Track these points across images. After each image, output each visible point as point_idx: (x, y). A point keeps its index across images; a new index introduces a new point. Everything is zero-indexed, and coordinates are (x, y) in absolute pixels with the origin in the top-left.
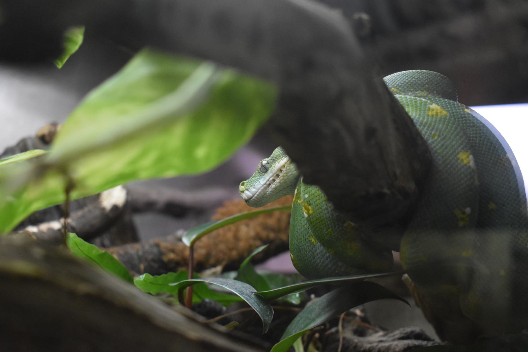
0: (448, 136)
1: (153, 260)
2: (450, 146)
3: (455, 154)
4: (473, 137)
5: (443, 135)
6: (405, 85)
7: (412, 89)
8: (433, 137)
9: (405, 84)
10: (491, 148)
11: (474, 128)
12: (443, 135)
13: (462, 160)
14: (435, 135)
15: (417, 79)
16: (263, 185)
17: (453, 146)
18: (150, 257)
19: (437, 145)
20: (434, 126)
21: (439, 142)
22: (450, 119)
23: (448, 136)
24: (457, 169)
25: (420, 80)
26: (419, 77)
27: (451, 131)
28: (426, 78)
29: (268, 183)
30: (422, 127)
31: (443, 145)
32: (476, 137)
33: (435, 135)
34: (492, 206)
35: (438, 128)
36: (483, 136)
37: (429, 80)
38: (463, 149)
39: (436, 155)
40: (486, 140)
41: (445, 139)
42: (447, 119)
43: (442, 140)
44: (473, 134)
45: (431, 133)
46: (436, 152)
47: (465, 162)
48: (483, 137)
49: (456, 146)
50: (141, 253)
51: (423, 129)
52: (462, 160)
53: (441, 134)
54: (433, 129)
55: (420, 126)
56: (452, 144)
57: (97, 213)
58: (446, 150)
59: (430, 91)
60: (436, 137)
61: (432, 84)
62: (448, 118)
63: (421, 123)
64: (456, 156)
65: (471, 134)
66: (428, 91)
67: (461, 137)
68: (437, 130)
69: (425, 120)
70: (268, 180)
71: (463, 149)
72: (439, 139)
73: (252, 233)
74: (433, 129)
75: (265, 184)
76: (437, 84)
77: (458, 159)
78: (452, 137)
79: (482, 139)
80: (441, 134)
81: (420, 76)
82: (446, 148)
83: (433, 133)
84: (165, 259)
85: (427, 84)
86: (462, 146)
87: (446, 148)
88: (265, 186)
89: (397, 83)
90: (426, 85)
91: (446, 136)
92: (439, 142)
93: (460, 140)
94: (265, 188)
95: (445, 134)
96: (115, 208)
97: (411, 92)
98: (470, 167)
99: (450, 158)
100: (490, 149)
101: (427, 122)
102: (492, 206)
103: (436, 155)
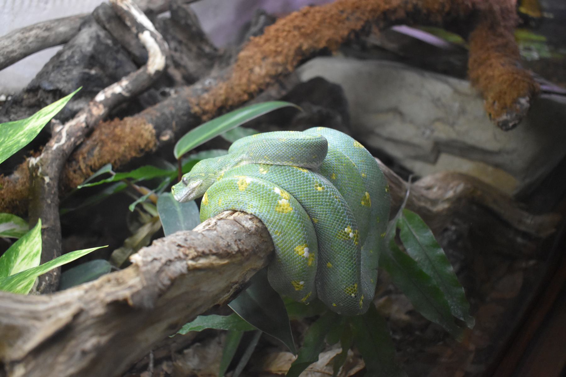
0: (289, 232)
1: (184, 115)
2: (289, 241)
3: (292, 247)
4: (320, 214)
5: (284, 231)
6: (275, 156)
7: (279, 160)
8: (276, 234)
9: (274, 156)
10: (334, 224)
11: (322, 206)
12: (284, 231)
13: (298, 252)
14: (277, 232)
15: (284, 152)
16: (185, 195)
17: (292, 241)
18: (181, 113)
19: (278, 240)
20: (278, 224)
21: (280, 238)
22: (292, 217)
23: (289, 232)
24: (293, 258)
25: (286, 154)
26: (286, 151)
27: (292, 228)
28: (292, 152)
29: (188, 194)
30: (268, 224)
31: (283, 240)
32: (322, 214)
33: (277, 232)
34: (329, 265)
35: (281, 225)
36: (328, 214)
37: (294, 154)
38: (299, 243)
39: (277, 247)
40: (330, 217)
41: (286, 235)
42: (290, 216)
43: (282, 236)
44: (320, 211)
45: (274, 230)
46: (277, 245)
47: (300, 253)
48: (328, 214)
49: (294, 241)
50: (173, 111)
51: (269, 225)
52: (298, 252)
53: (283, 231)
54: (277, 226)
55: (267, 223)
56: (291, 239)
57: (145, 77)
58: (286, 244)
59: (294, 162)
60: (278, 234)
61: (297, 156)
62: (291, 215)
63: (268, 221)
64: (293, 248)
65: (318, 212)
66: (293, 162)
67: (300, 233)
68: (280, 228)
69: (271, 218)
70: (188, 192)
71: (299, 243)
72: (281, 235)
73: (263, 72)
74: (277, 226)
75: (186, 194)
76: (301, 156)
77: (294, 251)
78: (291, 233)
79: (327, 216)
80: (283, 231)
81: (286, 149)
82: (286, 243)
83: (276, 230)
84: (192, 111)
85: (292, 157)
86: (298, 241)
87: (286, 243)
88: (186, 196)
89: (268, 153)
90: (291, 158)
91: (287, 232)
92: (280, 238)
93: (298, 236)
94: (187, 197)
95: (286, 231)
96: (157, 72)
97: (279, 161)
98: (303, 257)
99: (288, 250)
100: (332, 225)
101: (273, 220)
102: (329, 265)
103: (277, 247)
